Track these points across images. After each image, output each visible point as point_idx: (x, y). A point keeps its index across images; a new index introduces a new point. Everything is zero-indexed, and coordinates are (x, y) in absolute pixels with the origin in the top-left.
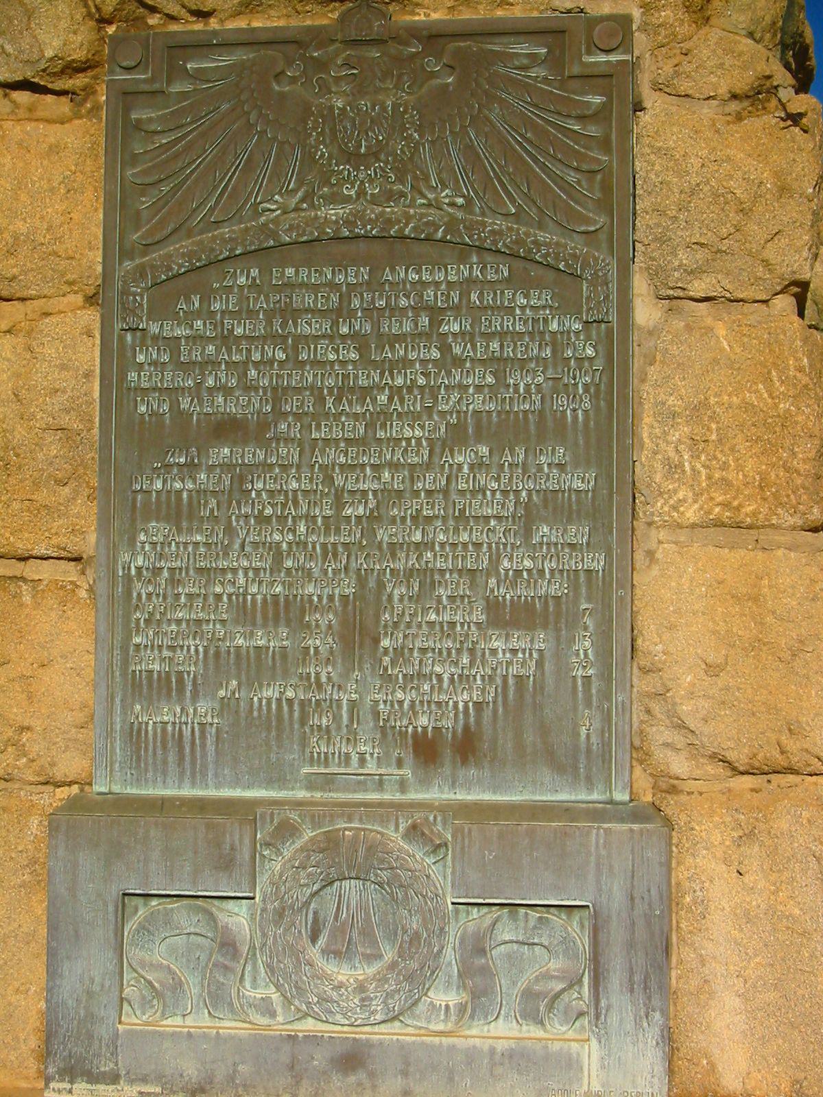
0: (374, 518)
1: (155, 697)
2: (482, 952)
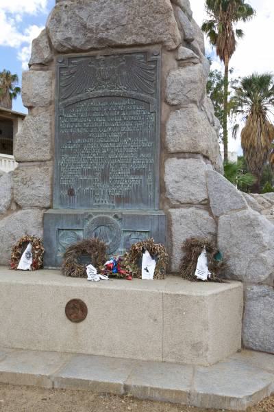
0: (108, 153)
2: (128, 240)
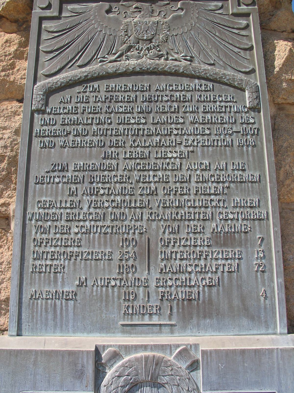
1: (42, 285)
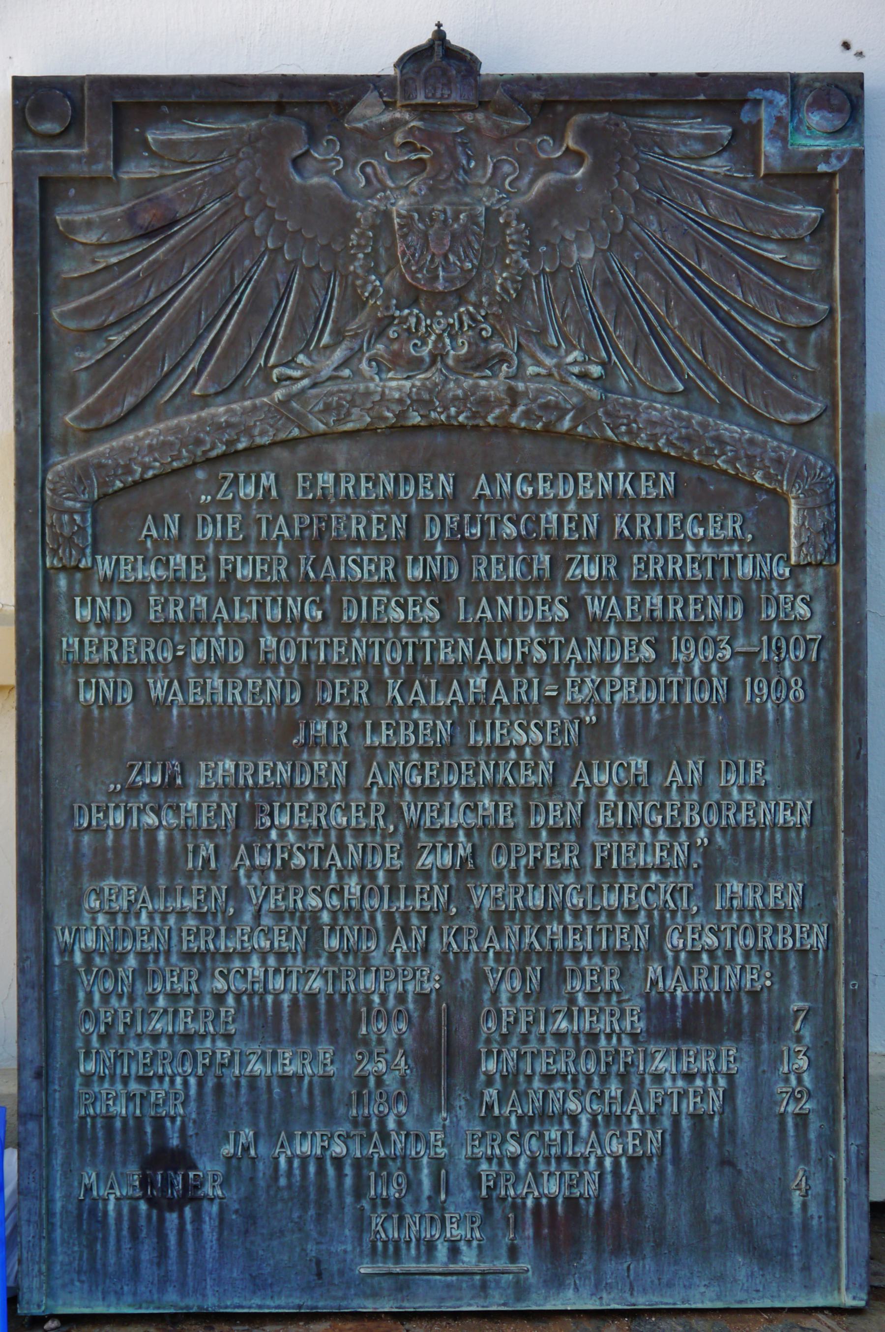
0: (468, 870)
